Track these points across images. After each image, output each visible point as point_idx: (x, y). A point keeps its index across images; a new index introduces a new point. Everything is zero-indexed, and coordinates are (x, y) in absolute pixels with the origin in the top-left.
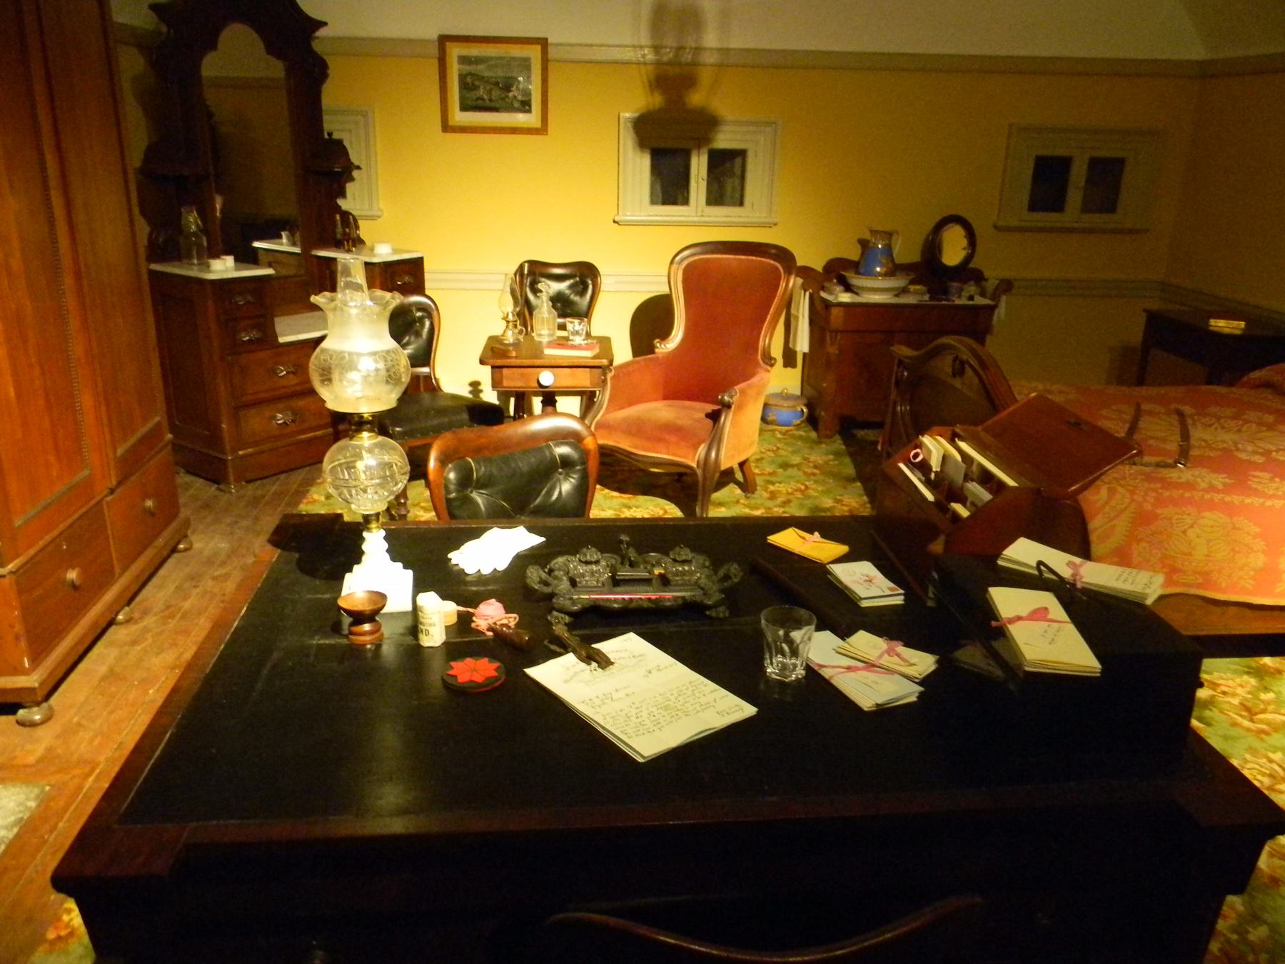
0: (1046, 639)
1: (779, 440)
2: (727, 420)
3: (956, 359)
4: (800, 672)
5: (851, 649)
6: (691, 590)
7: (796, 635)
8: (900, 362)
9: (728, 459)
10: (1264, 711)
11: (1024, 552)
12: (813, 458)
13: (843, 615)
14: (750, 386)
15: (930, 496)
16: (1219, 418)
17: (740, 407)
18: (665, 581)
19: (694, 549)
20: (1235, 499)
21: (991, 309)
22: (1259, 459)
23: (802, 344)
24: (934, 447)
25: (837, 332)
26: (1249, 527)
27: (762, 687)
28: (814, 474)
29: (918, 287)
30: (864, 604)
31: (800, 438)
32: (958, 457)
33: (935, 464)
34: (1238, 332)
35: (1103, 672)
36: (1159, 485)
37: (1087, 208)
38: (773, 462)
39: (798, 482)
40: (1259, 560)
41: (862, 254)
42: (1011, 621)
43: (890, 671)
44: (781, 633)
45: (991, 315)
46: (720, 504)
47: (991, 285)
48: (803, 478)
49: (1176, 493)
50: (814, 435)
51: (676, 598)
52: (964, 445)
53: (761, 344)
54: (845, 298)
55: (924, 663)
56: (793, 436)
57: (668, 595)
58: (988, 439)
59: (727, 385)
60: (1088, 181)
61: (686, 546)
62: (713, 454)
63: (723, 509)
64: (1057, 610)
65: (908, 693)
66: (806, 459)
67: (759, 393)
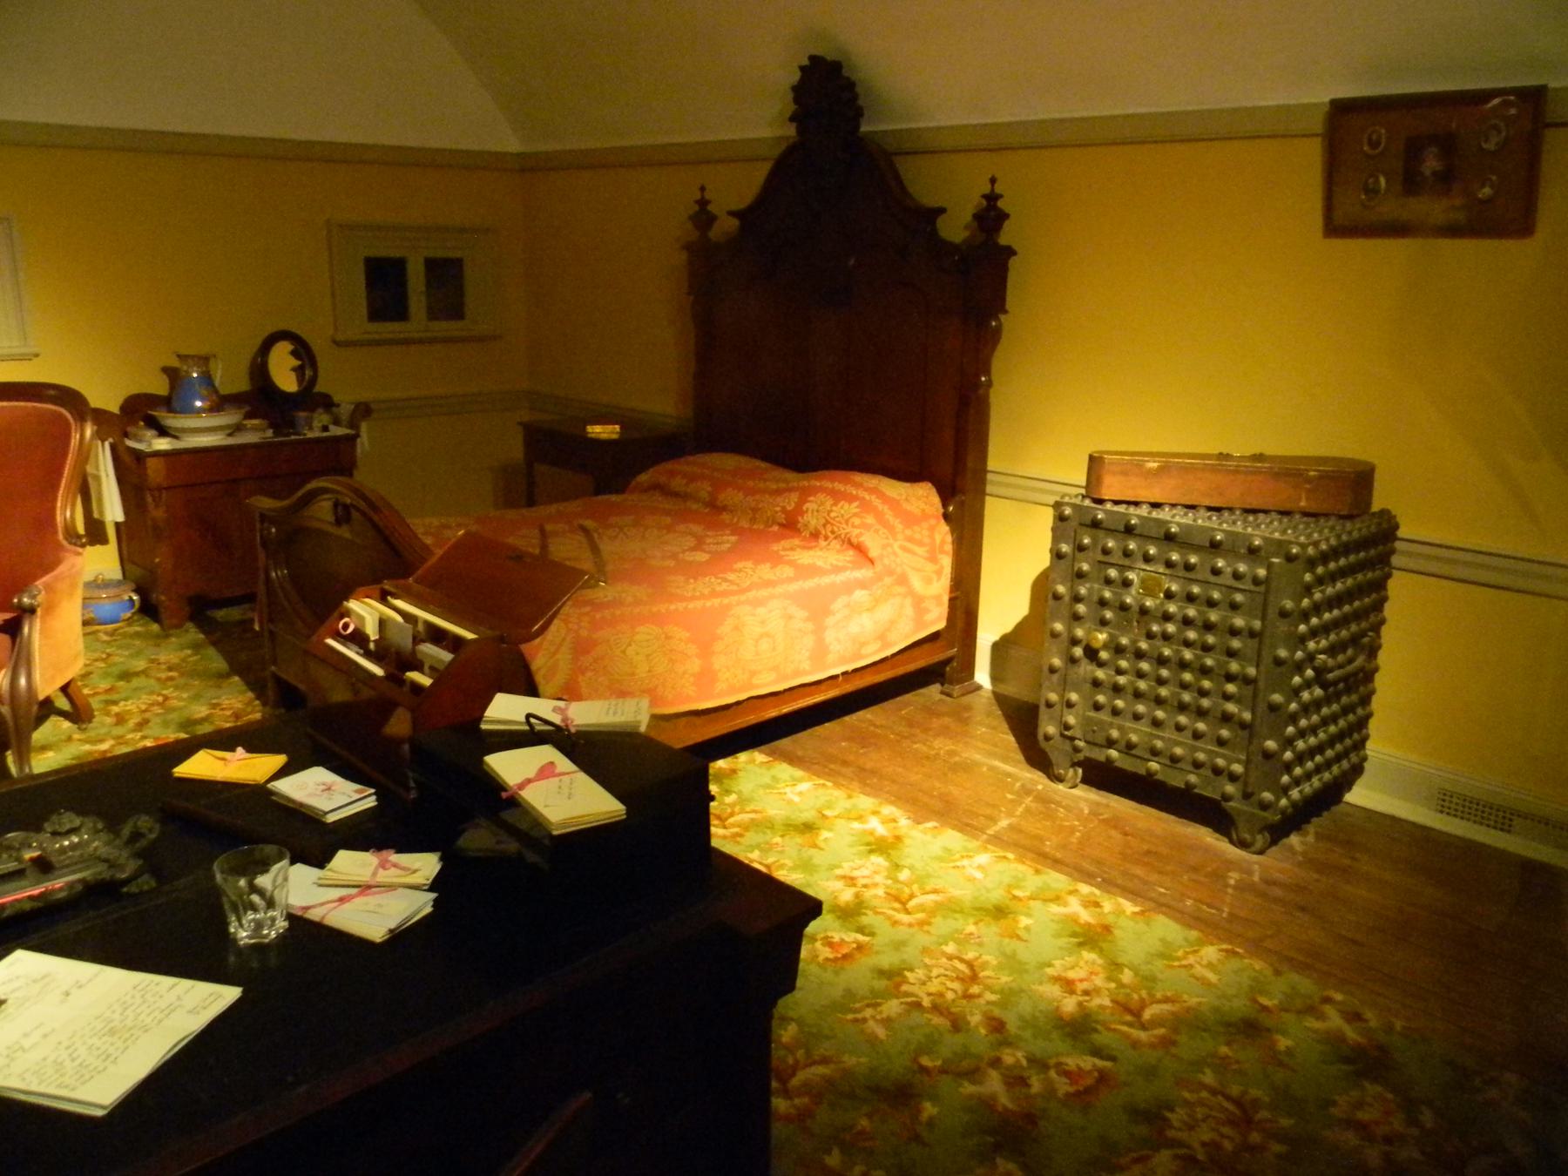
0: (567, 799)
1: (108, 643)
2: (34, 631)
3: (336, 505)
4: (282, 924)
5: (335, 876)
6: (88, 868)
7: (263, 881)
8: (263, 518)
9: (46, 684)
10: (732, 815)
11: (506, 709)
12: (162, 658)
13: (314, 840)
14: (56, 579)
15: (378, 671)
16: (621, 529)
17: (50, 608)
18: (44, 866)
19: (81, 812)
20: (663, 608)
21: (351, 440)
22: (672, 563)
23: (113, 510)
24: (365, 612)
25: (160, 489)
26: (680, 633)
27: (232, 959)
28: (171, 679)
29: (256, 422)
30: (331, 818)
31: (137, 635)
32: (399, 619)
33: (372, 631)
34: (615, 436)
35: (628, 813)
36: (588, 609)
37: (433, 315)
38: (106, 675)
39: (152, 693)
40: (695, 665)
41: (172, 388)
42: (522, 786)
43: (391, 887)
44: (242, 882)
45: (354, 446)
46: (44, 748)
47: (345, 410)
48: (157, 687)
49: (607, 613)
50: (155, 627)
51: (71, 885)
52: (399, 603)
53: (59, 519)
54: (162, 444)
55: (426, 865)
56: (125, 635)
57: (58, 883)
58: (417, 588)
59: (23, 584)
60: (429, 284)
61: (67, 810)
62: (23, 681)
63: (50, 754)
64: (563, 763)
65: (422, 904)
66: (152, 661)
67: (73, 586)
